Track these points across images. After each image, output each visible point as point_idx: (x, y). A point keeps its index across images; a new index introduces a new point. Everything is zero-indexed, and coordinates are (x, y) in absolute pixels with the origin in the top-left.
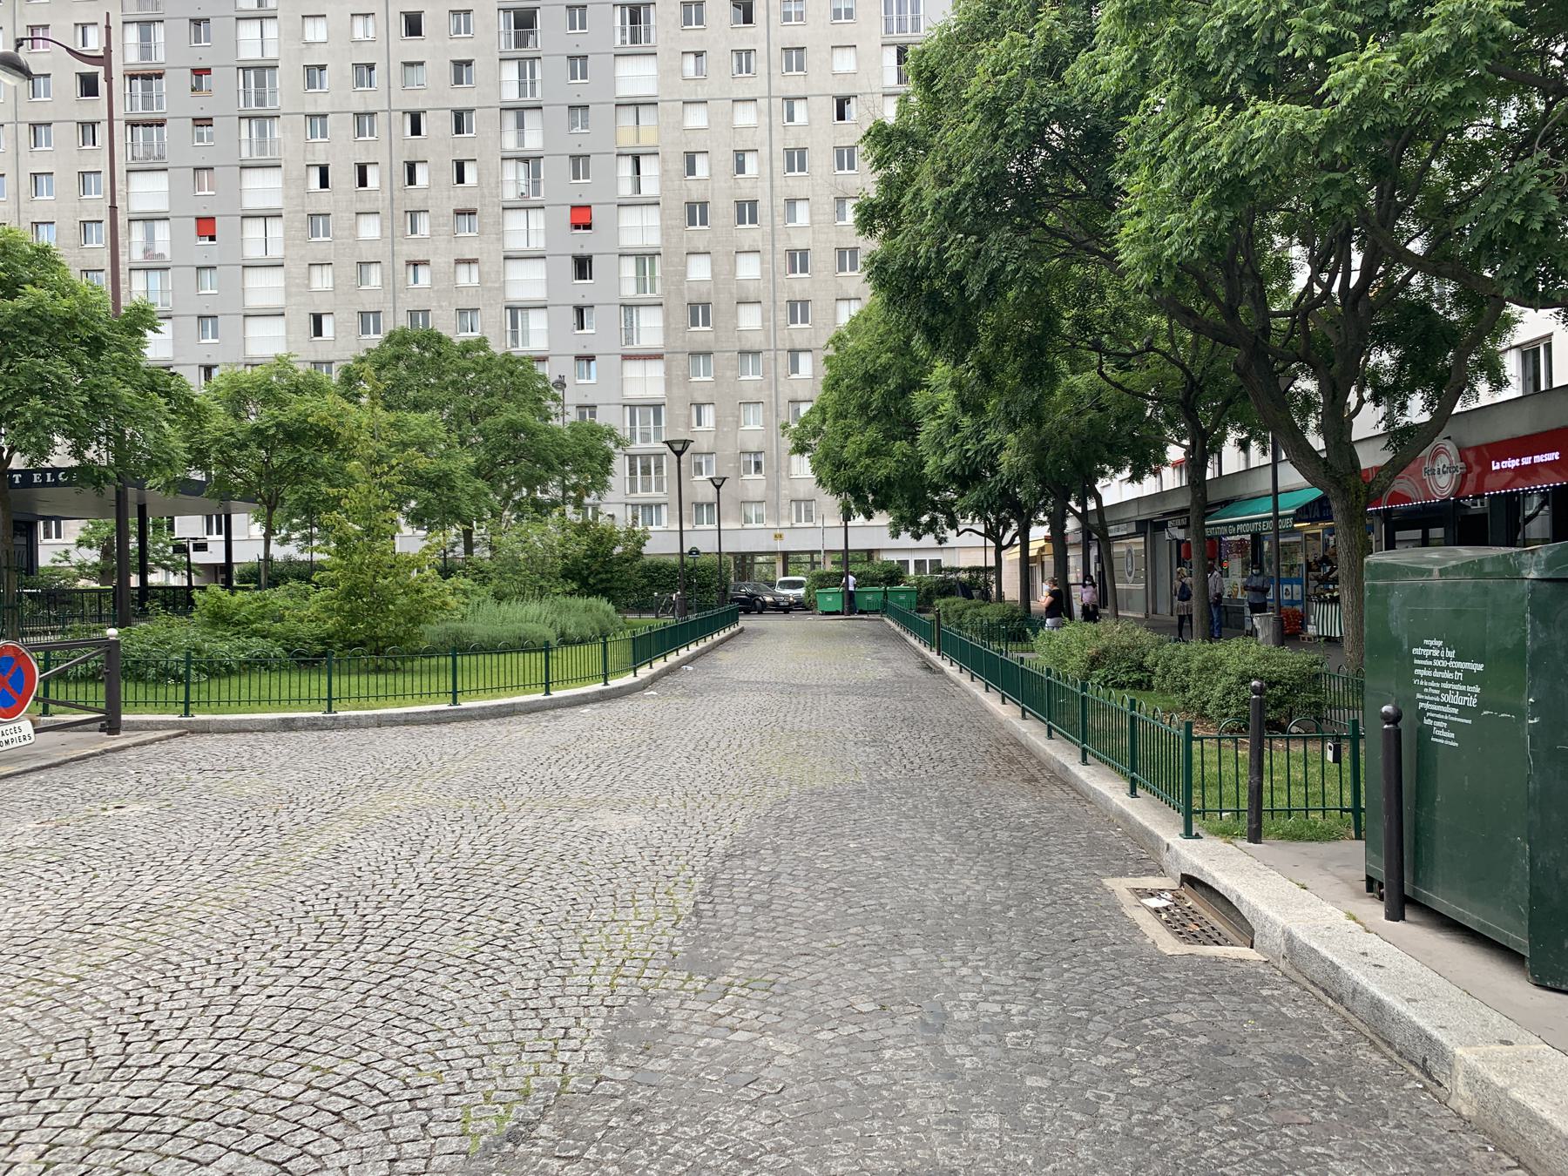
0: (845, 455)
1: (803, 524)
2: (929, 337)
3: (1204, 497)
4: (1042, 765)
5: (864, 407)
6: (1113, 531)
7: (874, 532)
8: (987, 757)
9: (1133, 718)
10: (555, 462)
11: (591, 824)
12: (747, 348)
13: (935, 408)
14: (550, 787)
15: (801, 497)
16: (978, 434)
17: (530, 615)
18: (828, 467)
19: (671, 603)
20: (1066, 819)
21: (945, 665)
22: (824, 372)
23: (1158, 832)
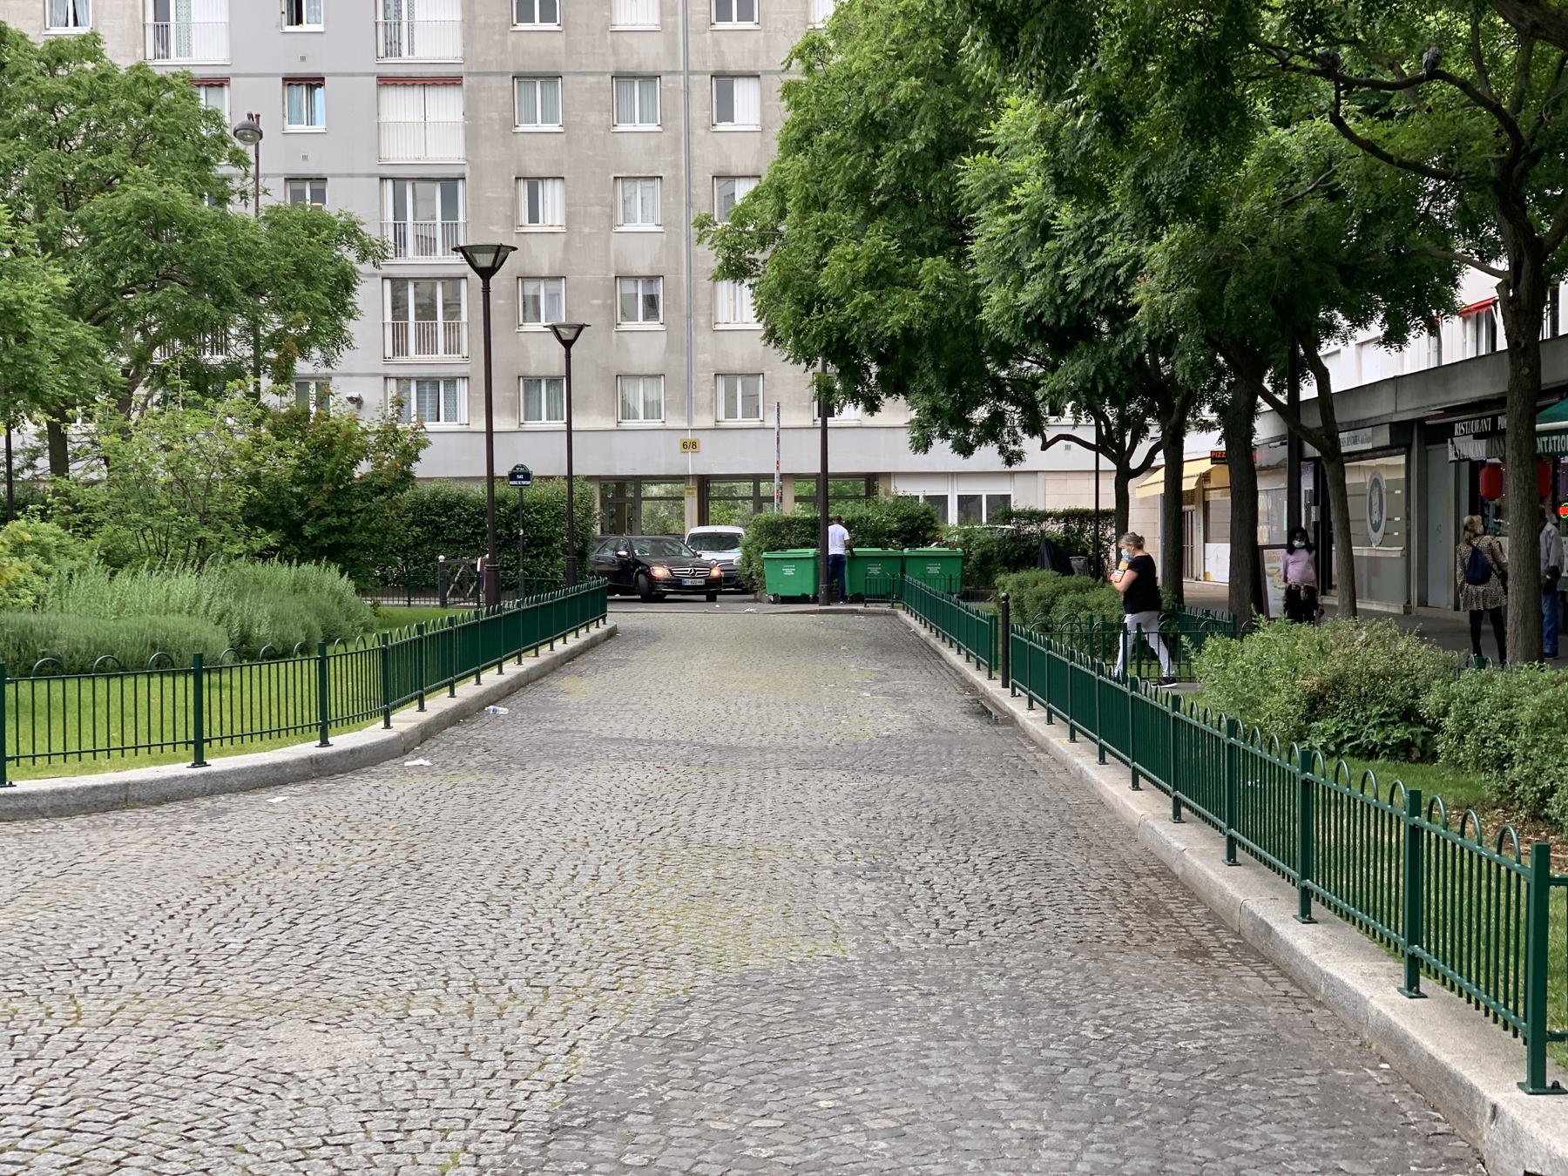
0: (823, 282)
1: (740, 421)
2: (995, 37)
3: (1535, 375)
4: (1217, 919)
5: (860, 188)
6: (1348, 443)
7: (880, 439)
8: (1105, 903)
9: (1415, 832)
10: (235, 288)
11: (262, 1055)
12: (630, 66)
13: (1002, 193)
14: (185, 970)
15: (736, 366)
16: (1088, 243)
17: (173, 599)
18: (787, 307)
19: (471, 576)
20: (1272, 1042)
21: (1017, 706)
22: (782, 114)
23: (1471, 1075)
